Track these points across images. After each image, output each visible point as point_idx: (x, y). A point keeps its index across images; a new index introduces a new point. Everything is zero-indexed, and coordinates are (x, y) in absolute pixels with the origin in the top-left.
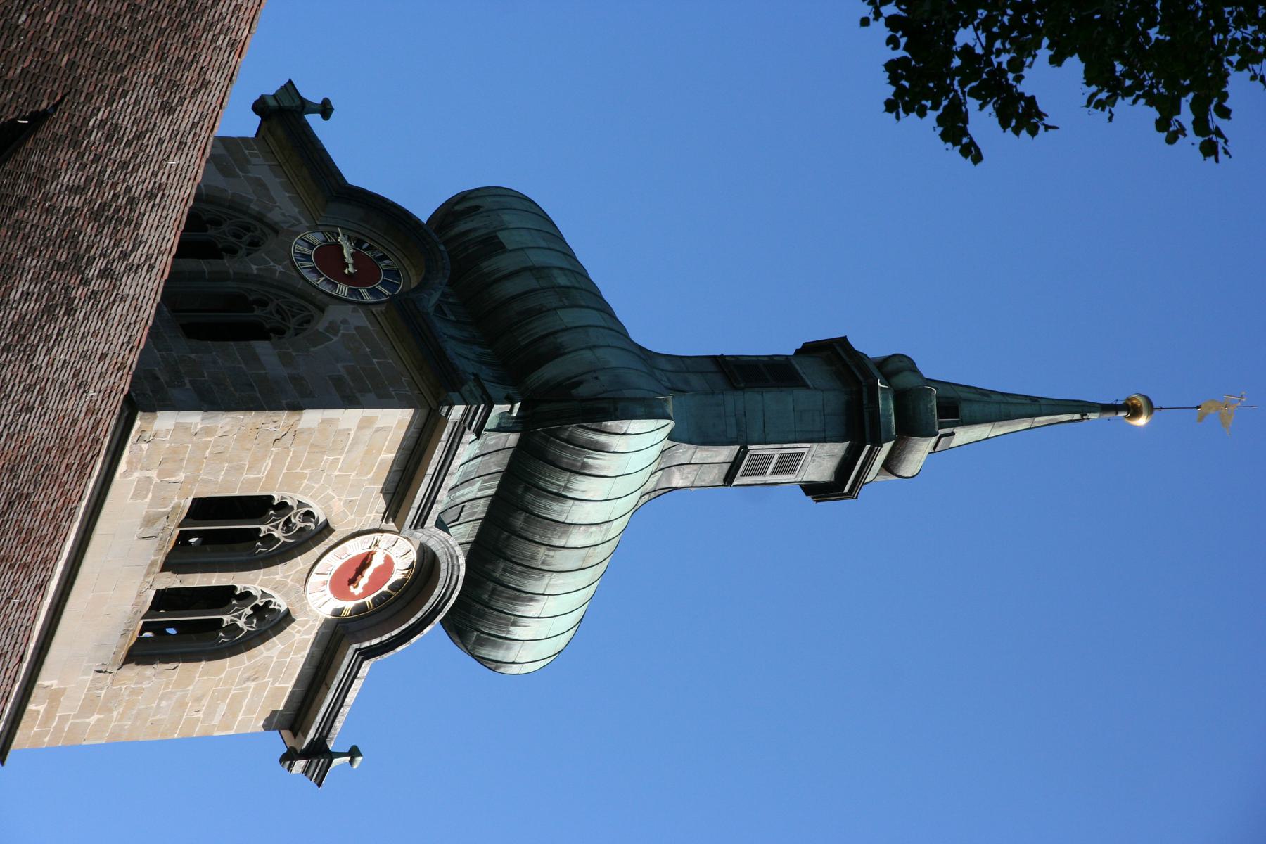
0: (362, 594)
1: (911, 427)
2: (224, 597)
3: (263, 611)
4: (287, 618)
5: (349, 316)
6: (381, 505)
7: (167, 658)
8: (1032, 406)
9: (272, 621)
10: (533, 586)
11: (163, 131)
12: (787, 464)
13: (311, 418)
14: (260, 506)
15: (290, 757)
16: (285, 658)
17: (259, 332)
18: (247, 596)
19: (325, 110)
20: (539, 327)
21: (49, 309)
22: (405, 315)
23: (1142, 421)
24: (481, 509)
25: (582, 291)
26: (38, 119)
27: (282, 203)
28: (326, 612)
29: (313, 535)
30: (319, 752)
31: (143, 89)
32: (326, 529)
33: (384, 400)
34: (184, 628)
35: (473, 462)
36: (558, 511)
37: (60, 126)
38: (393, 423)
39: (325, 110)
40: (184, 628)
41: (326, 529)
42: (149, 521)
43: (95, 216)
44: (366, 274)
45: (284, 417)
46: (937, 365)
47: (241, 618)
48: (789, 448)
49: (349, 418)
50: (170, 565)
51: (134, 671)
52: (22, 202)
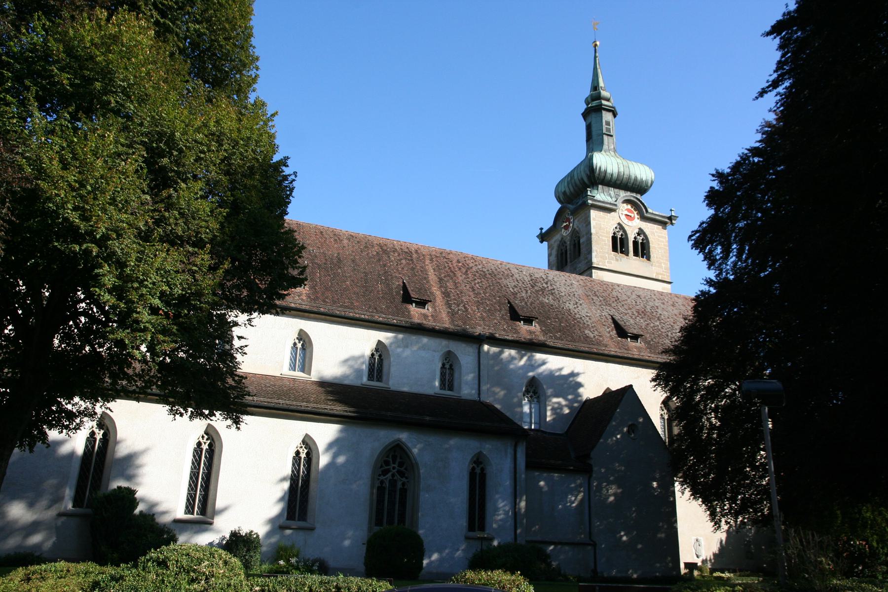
0: (635, 214)
1: (598, 97)
2: (635, 243)
3: (639, 234)
4: (640, 229)
5: (575, 223)
6: (613, 213)
7: (649, 252)
8: (595, 69)
9: (641, 232)
10: (633, 177)
11: (517, 276)
12: (608, 123)
13: (593, 231)
14: (614, 238)
15: (672, 224)
16: (648, 228)
17: (579, 241)
18: (635, 238)
19: (541, 229)
20: (578, 182)
21: (552, 294)
22: (574, 213)
23: (598, 43)
24: (617, 190)
25: (571, 175)
26: (509, 302)
27: (557, 238)
28: (639, 221)
29: (621, 227)
30: (670, 218)
31: (504, 282)
32: (619, 224)
33: (589, 216)
34: (642, 249)
35: (601, 195)
36: (615, 175)
37: (511, 298)
38: (594, 213)
39: (541, 229)
40: (642, 249)
41: (619, 224)
42: (617, 260)
43: (533, 287)
44: (568, 220)
45: (593, 236)
46: (587, 92)
47: (640, 239)
48: (604, 123)
49: (593, 223)
50: (627, 255)
51: (652, 259)
52: (526, 303)
